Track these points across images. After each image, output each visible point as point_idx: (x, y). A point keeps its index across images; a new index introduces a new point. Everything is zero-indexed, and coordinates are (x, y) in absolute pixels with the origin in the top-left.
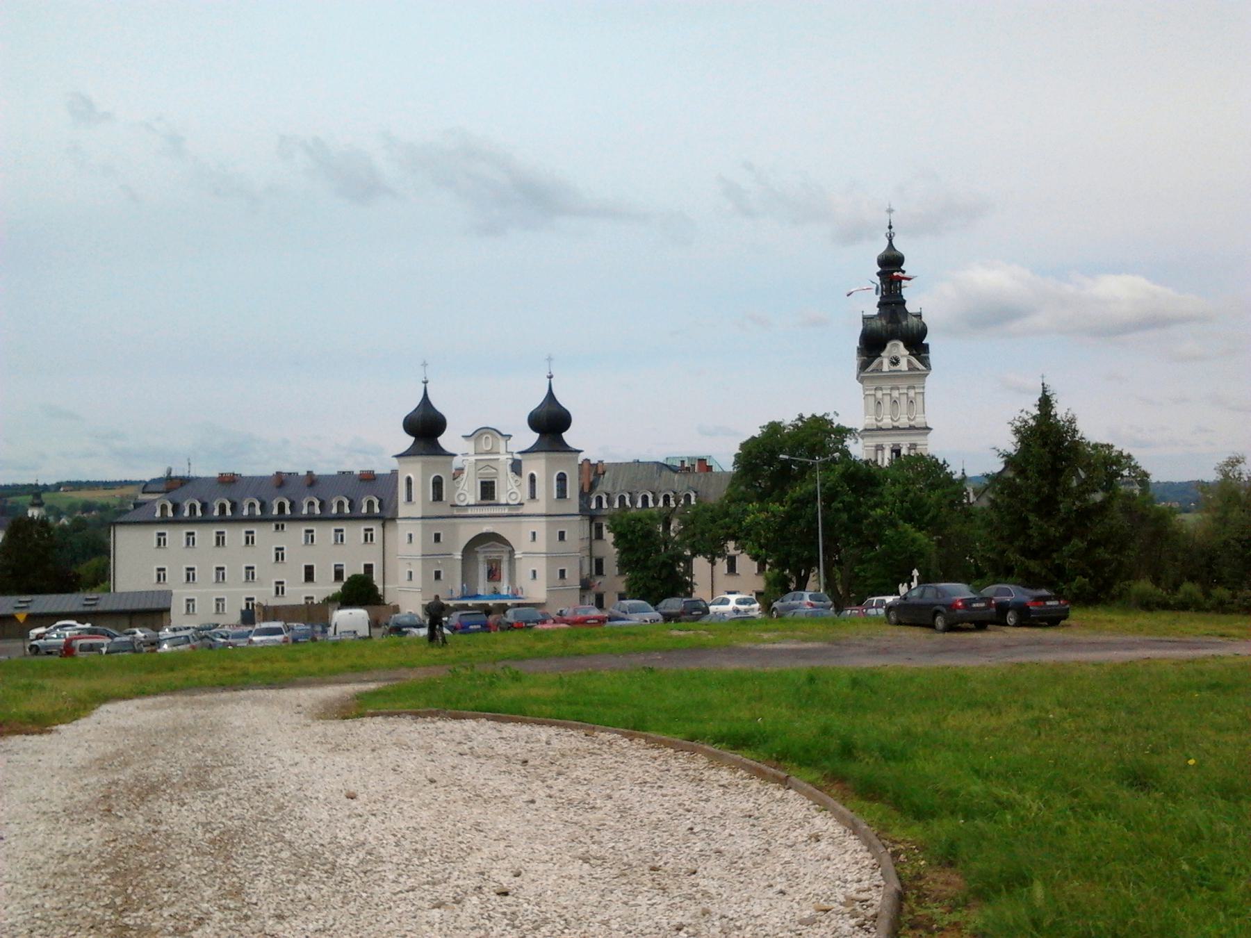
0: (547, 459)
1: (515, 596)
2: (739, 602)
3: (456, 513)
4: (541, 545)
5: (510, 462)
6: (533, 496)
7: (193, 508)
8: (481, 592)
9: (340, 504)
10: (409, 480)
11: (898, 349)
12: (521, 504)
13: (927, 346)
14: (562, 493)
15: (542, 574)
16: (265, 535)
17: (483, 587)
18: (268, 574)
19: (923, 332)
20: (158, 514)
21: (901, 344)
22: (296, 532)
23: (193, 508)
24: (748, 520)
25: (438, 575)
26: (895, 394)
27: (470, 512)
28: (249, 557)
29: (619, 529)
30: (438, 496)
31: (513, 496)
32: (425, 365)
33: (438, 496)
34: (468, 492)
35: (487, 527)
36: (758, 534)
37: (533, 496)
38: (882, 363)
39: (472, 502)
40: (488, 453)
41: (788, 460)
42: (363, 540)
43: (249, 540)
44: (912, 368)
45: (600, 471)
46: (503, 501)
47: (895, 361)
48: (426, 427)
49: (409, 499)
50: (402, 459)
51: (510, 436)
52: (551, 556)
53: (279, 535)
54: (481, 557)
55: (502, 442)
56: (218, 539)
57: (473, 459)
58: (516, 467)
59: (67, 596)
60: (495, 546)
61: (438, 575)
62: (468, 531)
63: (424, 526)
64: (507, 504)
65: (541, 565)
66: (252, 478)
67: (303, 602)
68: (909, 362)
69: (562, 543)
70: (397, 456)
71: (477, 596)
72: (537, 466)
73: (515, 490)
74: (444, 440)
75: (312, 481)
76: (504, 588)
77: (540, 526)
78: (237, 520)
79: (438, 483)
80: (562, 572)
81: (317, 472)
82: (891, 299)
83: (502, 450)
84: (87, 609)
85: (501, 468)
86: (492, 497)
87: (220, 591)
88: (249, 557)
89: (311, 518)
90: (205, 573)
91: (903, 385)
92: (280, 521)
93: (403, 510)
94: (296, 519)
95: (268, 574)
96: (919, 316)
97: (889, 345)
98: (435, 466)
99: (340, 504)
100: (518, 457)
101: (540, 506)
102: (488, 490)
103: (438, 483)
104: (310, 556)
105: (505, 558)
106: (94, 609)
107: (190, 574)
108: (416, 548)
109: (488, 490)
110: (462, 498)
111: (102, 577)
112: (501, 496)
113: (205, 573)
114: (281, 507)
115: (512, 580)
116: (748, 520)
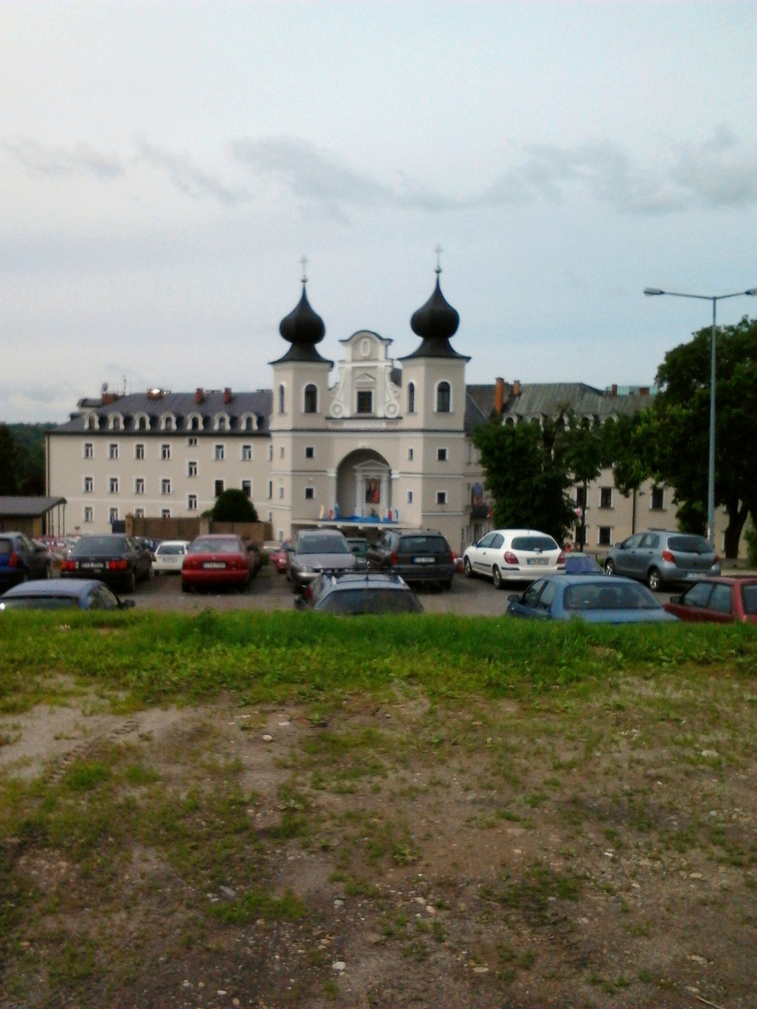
0: (428, 366)
1: (389, 520)
2: (519, 544)
3: (330, 426)
4: (418, 465)
5: (389, 370)
6: (411, 409)
7: (142, 421)
8: (358, 513)
9: (249, 420)
12: (399, 418)
14: (444, 407)
15: (418, 498)
16: (179, 447)
17: (360, 508)
20: (86, 426)
22: (206, 448)
23: (142, 421)
24: (639, 430)
25: (309, 493)
27: (347, 425)
29: (484, 445)
30: (311, 407)
31: (392, 409)
33: (311, 407)
34: (344, 405)
35: (363, 443)
36: (651, 450)
37: (411, 409)
39: (347, 413)
40: (367, 359)
45: (516, 391)
46: (380, 414)
48: (303, 331)
49: (282, 411)
50: (280, 366)
51: (390, 341)
52: (427, 477)
54: (359, 477)
55: (381, 348)
56: (138, 452)
57: (349, 366)
58: (396, 377)
60: (374, 465)
61: (309, 493)
62: (343, 447)
63: (294, 438)
64: (385, 418)
65: (416, 486)
66: (178, 396)
67: (160, 515)
69: (442, 463)
70: (273, 363)
71: (353, 518)
72: (416, 374)
73: (394, 402)
74: (323, 348)
75: (229, 398)
76: (383, 513)
77: (417, 442)
78: (155, 433)
79: (311, 393)
80: (441, 497)
81: (234, 390)
83: (381, 356)
85: (379, 377)
86: (369, 410)
88: (112, 470)
89: (221, 434)
90: (101, 484)
92: (193, 436)
94: (208, 434)
98: (309, 373)
99: (249, 420)
100: (398, 365)
101: (417, 421)
102: (364, 401)
103: (311, 393)
105: (385, 478)
109: (364, 401)
110: (337, 410)
112: (379, 409)
113: (101, 484)
114: (195, 423)
115: (390, 503)
116: (639, 430)
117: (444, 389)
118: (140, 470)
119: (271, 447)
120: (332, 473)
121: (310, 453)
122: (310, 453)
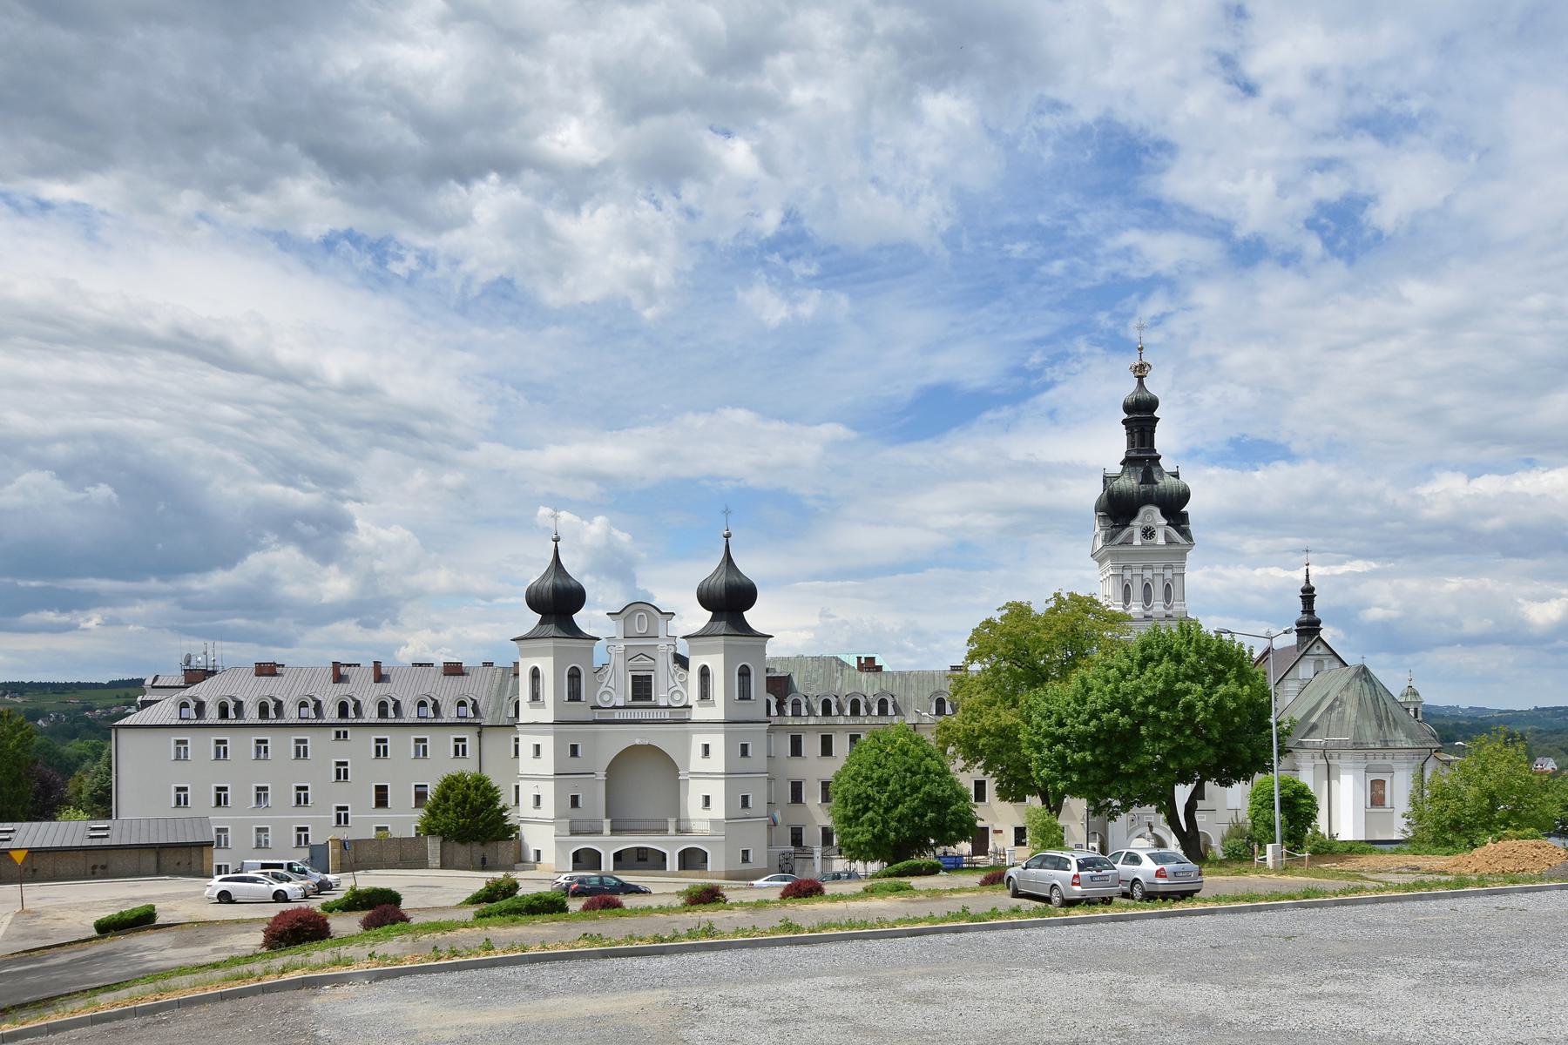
10: (535, 674)
11: (1153, 516)
13: (1186, 514)
14: (745, 695)
18: (325, 795)
19: (1185, 496)
21: (1157, 511)
22: (361, 744)
26: (1148, 574)
27: (617, 715)
28: (301, 773)
30: (575, 695)
32: (727, 512)
33: (575, 695)
34: (620, 692)
38: (1132, 534)
41: (1024, 651)
42: (373, 754)
43: (301, 752)
44: (1169, 541)
47: (1148, 533)
48: (558, 604)
49: (535, 696)
53: (341, 744)
59: (45, 824)
62: (618, 740)
63: (556, 735)
64: (669, 707)
67: (373, 835)
68: (1167, 535)
74: (579, 618)
79: (575, 675)
80: (745, 799)
82: (1142, 454)
83: (662, 635)
84: (96, 842)
87: (263, 818)
88: (301, 773)
91: (1158, 563)
93: (527, 714)
95: (325, 795)
96: (1176, 475)
97: (1142, 511)
102: (642, 687)
103: (575, 675)
104: (382, 773)
106: (105, 842)
107: (221, 798)
108: (547, 765)
109: (642, 687)
110: (606, 698)
111: (102, 803)
112: (661, 695)
113: (242, 795)
117: (745, 673)
118: (262, 774)
119: (517, 740)
120: (601, 776)
121: (574, 750)
122: (574, 750)
